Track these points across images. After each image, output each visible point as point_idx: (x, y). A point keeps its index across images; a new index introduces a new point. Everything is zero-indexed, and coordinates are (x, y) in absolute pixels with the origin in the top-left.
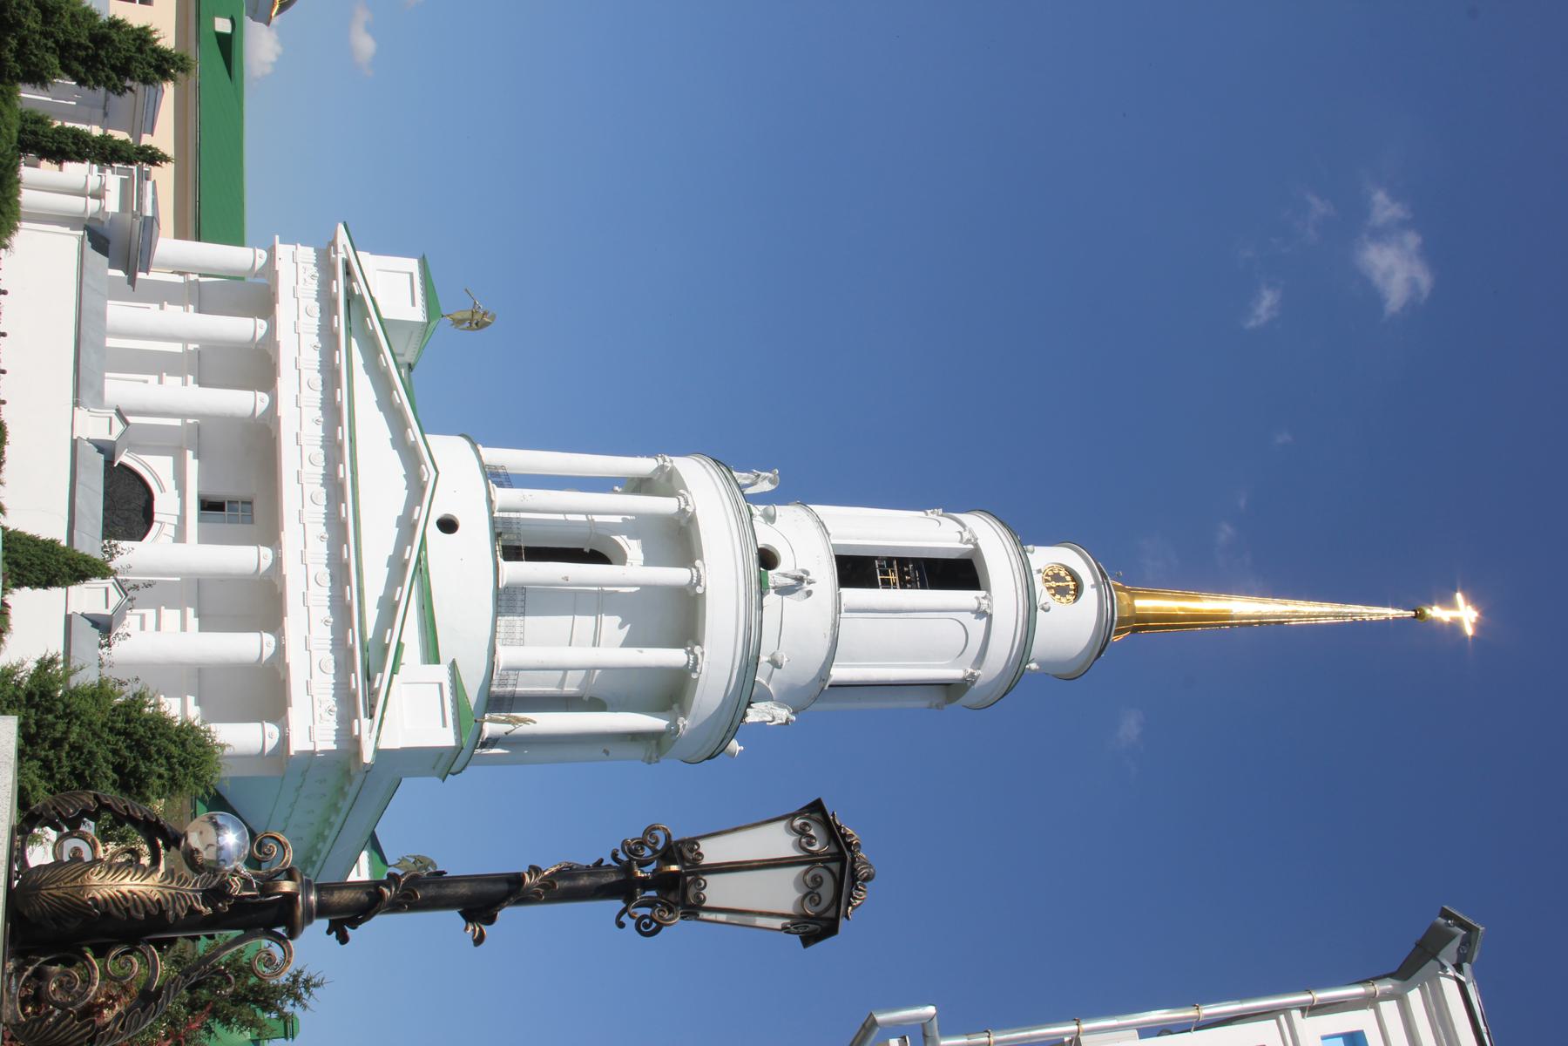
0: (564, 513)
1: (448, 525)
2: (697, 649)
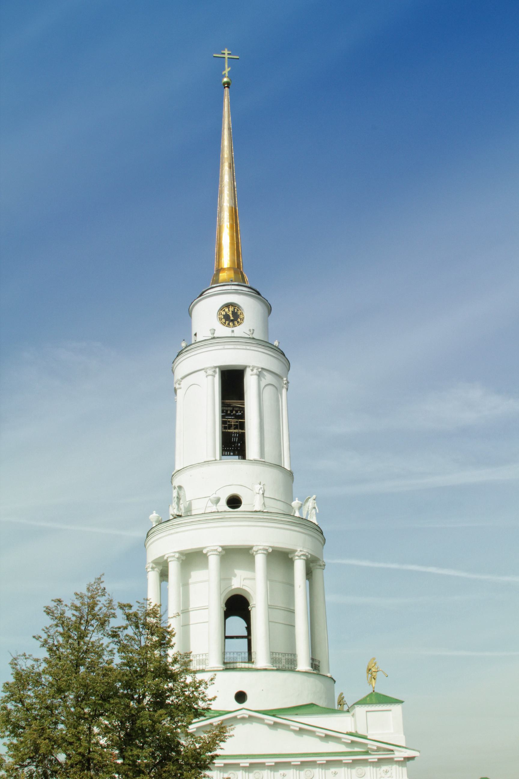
1: (241, 697)
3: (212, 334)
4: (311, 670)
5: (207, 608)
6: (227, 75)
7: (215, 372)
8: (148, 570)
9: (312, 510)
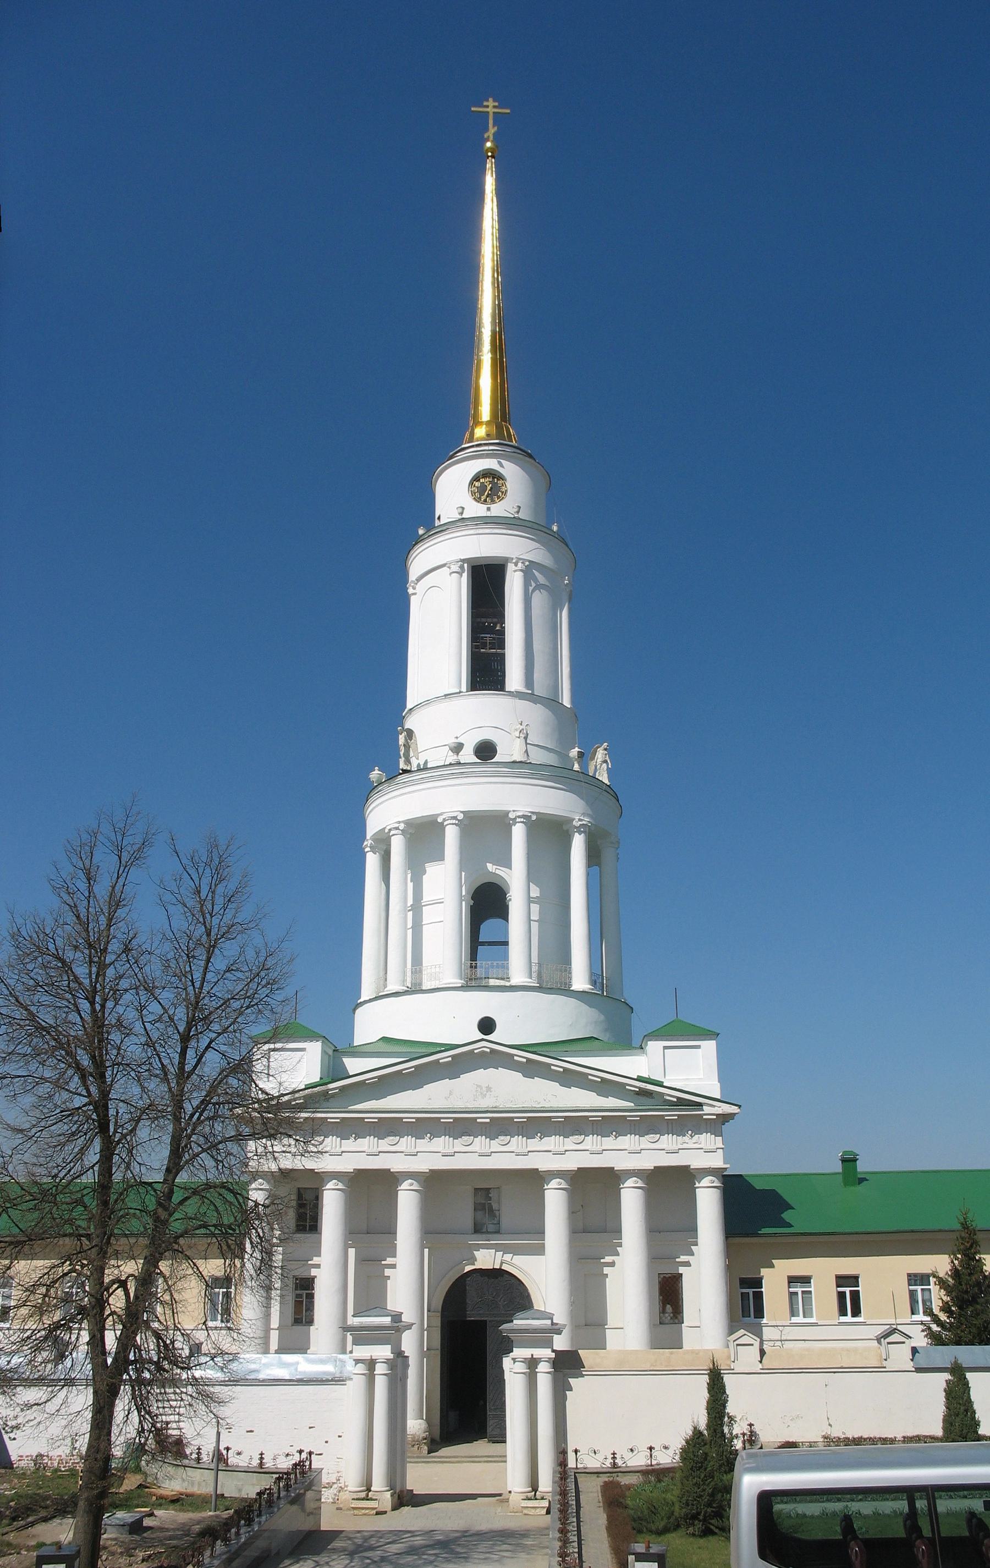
0: (406, 929)
1: (487, 1026)
2: (511, 816)
3: (459, 514)
4: (593, 989)
5: (442, 902)
6: (491, 138)
7: (462, 567)
8: (366, 850)
9: (601, 765)
